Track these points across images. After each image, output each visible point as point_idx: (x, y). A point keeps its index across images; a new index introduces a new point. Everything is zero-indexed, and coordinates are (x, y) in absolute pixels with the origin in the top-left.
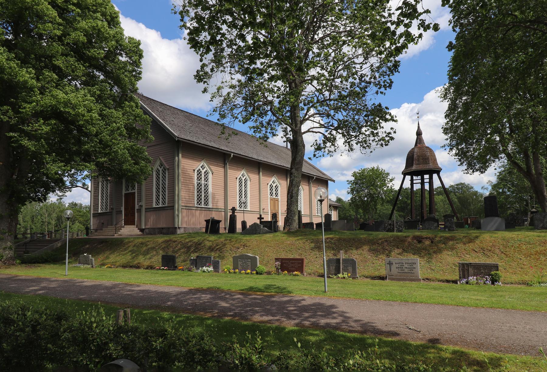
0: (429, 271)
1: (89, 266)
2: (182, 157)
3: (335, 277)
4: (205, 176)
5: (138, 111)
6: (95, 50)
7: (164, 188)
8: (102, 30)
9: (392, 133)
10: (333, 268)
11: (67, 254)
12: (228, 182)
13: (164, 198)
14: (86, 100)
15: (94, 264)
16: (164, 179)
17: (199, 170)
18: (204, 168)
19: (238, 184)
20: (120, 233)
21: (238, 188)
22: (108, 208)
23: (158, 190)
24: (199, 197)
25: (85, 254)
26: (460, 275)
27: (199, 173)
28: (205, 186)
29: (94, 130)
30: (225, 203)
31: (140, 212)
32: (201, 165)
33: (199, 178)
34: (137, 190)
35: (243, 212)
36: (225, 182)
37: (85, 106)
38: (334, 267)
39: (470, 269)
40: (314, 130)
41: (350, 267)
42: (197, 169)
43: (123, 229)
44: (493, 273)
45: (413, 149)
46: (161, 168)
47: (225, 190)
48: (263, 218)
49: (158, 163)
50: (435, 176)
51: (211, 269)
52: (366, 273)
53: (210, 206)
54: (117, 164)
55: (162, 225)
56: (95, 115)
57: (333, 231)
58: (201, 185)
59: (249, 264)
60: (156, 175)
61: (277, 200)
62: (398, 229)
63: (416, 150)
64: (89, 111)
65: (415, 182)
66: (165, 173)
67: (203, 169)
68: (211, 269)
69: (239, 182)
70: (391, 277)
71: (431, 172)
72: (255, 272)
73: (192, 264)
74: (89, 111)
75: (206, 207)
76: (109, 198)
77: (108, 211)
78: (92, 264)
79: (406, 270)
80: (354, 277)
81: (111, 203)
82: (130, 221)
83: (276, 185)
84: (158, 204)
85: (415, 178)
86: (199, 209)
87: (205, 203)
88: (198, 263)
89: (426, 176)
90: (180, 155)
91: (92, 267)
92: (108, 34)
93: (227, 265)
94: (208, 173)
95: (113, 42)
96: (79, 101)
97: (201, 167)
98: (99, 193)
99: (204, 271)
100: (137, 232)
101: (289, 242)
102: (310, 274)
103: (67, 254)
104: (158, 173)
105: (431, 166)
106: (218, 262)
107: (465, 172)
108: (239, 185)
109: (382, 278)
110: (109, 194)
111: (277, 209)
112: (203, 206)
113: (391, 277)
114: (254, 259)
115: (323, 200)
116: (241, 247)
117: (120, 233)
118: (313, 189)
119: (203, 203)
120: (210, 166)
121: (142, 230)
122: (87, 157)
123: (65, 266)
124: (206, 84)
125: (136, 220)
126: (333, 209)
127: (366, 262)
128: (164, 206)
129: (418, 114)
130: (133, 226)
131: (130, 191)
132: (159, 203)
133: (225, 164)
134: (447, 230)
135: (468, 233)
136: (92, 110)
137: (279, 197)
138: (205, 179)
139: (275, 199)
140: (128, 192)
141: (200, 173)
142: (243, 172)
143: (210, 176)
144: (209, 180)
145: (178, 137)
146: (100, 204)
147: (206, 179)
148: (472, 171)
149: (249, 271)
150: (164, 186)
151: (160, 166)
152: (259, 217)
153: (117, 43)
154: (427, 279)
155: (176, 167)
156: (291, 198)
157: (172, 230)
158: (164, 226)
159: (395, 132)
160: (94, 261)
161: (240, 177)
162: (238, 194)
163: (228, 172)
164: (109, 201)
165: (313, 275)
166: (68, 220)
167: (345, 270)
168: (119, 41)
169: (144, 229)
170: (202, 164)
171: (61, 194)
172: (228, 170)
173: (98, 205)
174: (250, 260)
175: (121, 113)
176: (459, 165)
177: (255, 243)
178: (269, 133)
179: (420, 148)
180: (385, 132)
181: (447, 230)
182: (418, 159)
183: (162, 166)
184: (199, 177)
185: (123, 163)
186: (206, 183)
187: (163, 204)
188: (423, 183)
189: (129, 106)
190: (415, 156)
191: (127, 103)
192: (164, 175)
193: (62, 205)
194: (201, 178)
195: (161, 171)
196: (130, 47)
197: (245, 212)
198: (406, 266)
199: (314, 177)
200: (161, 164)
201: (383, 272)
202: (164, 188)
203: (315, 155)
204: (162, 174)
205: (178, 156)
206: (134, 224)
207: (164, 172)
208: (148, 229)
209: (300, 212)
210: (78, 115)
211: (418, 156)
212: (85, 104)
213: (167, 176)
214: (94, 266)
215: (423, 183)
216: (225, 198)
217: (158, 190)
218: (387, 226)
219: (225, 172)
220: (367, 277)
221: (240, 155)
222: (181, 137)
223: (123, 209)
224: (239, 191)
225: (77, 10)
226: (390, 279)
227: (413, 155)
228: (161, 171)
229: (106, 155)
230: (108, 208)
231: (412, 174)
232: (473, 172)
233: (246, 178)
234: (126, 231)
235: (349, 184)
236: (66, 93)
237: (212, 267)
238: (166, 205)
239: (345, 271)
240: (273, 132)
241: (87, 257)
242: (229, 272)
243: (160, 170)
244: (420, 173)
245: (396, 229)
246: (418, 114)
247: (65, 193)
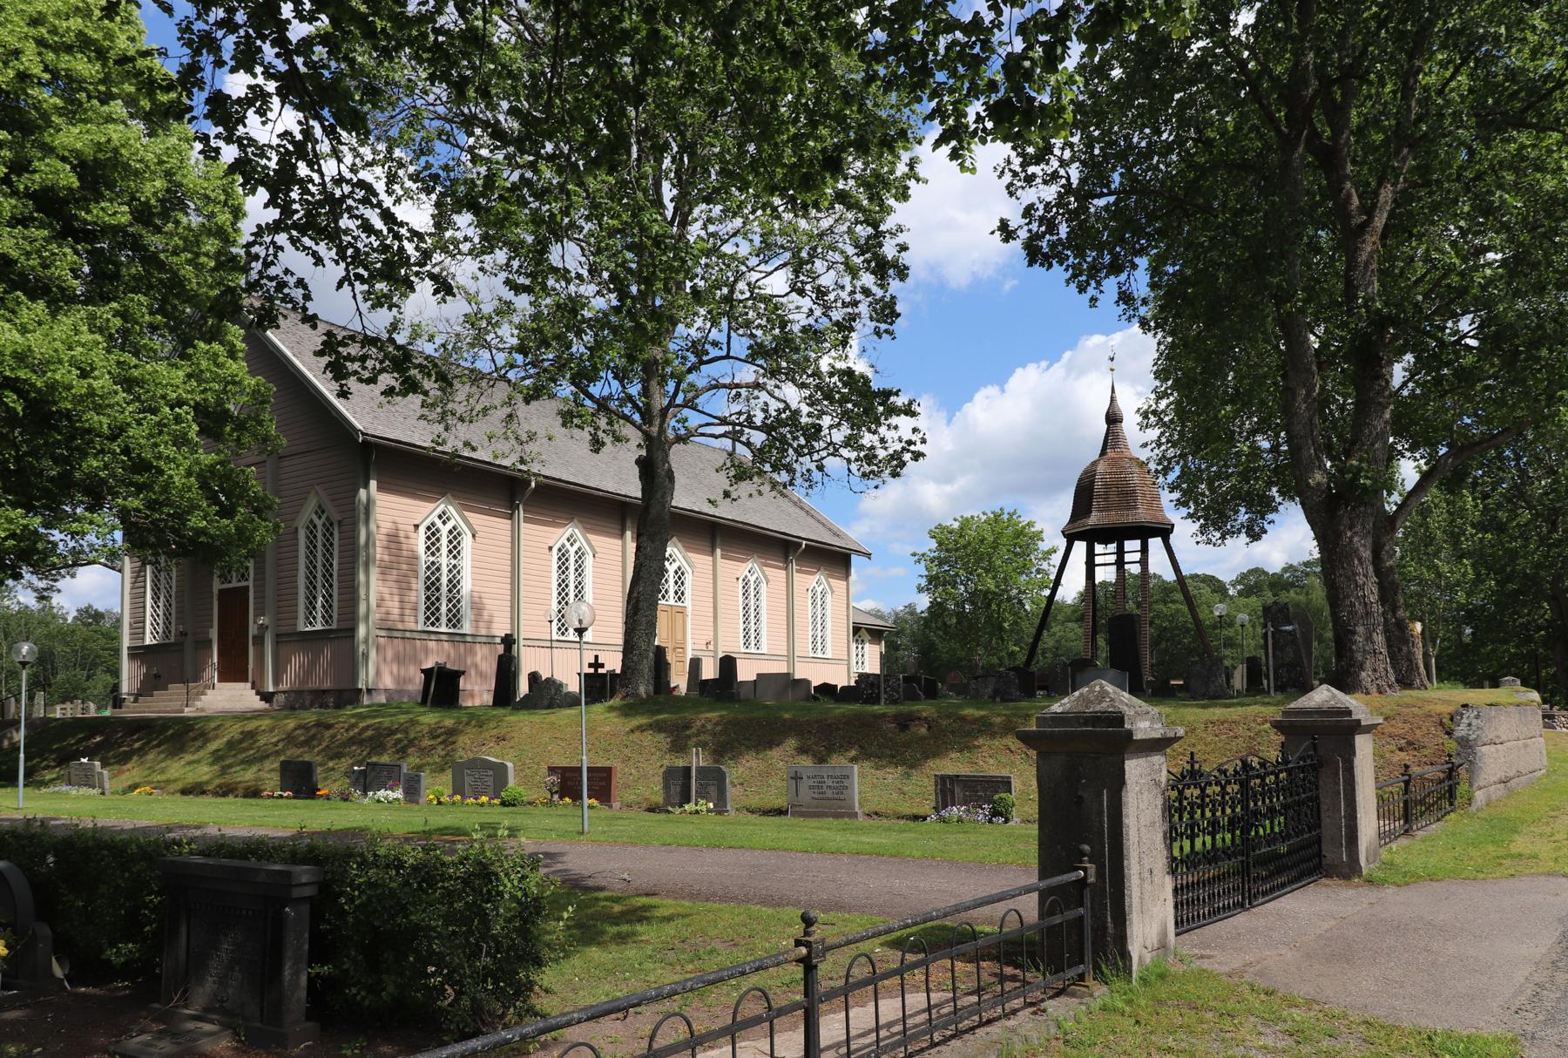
0: (895, 796)
1: (96, 791)
2: (380, 489)
4: (450, 542)
5: (234, 366)
6: (103, 204)
7: (328, 575)
8: (123, 151)
10: (676, 789)
11: (22, 755)
12: (522, 559)
13: (328, 607)
14: (79, 343)
15: (107, 786)
16: (328, 550)
17: (433, 524)
18: (448, 519)
20: (199, 704)
21: (555, 575)
22: (173, 632)
23: (311, 583)
24: (433, 604)
25: (85, 760)
27: (432, 533)
28: (450, 571)
29: (102, 422)
30: (512, 619)
31: (262, 644)
32: (439, 511)
34: (255, 580)
35: (578, 646)
36: (512, 560)
37: (73, 362)
38: (678, 789)
39: (957, 790)
41: (712, 788)
42: (427, 523)
45: (1094, 463)
46: (320, 518)
47: (512, 584)
48: (602, 666)
49: (312, 504)
50: (1155, 543)
51: (398, 794)
52: (755, 801)
53: (467, 628)
54: (169, 515)
58: (438, 569)
59: (490, 781)
60: (308, 537)
61: (682, 612)
62: (890, 696)
63: (1101, 468)
64: (84, 375)
65: (1098, 560)
66: (332, 534)
67: (444, 523)
68: (398, 794)
69: (560, 559)
72: (496, 801)
74: (84, 375)
75: (451, 631)
76: (173, 603)
77: (173, 640)
78: (101, 786)
79: (829, 793)
81: (180, 620)
82: (233, 670)
83: (679, 568)
84: (311, 623)
85: (1099, 548)
86: (433, 637)
88: (367, 780)
89: (1132, 545)
91: (103, 793)
92: (141, 161)
94: (459, 534)
95: (158, 184)
96: (56, 351)
98: (145, 587)
100: (256, 703)
101: (608, 729)
102: (629, 806)
103: (22, 755)
104: (311, 532)
105: (1142, 515)
106: (417, 780)
107: (1199, 539)
108: (560, 568)
109: (780, 812)
110: (174, 589)
111: (679, 636)
112: (443, 629)
114: (500, 770)
115: (586, 629)
117: (199, 704)
118: (799, 578)
119: (444, 620)
120: (466, 513)
121: (266, 697)
123: (15, 789)
125: (251, 666)
126: (867, 637)
128: (327, 627)
129: (1112, 359)
130: (242, 685)
131: (234, 584)
132: (314, 618)
134: (998, 699)
135: (1016, 708)
137: (688, 601)
138: (450, 552)
139: (675, 609)
140: (230, 586)
141: (433, 534)
142: (570, 530)
144: (463, 553)
145: (363, 434)
146: (148, 619)
147: (454, 551)
148: (1218, 535)
149: (484, 799)
151: (316, 513)
154: (876, 814)
156: (635, 614)
157: (348, 695)
158: (327, 685)
159: (924, 441)
160: (106, 779)
161: (563, 546)
162: (555, 593)
163: (522, 531)
164: (173, 612)
165: (636, 808)
166: (24, 668)
167: (702, 794)
168: (174, 174)
170: (442, 507)
171: (42, 584)
172: (523, 524)
173: (144, 622)
174: (491, 773)
176: (868, 555)
177: (526, 730)
179: (1114, 463)
180: (900, 440)
181: (998, 699)
182: (1106, 493)
183: (323, 512)
184: (433, 544)
187: (327, 622)
188: (1120, 563)
190: (1098, 484)
192: (328, 540)
193: (54, 617)
194: (438, 550)
195: (320, 528)
197: (549, 644)
199: (800, 544)
200: (320, 507)
201: (780, 802)
202: (328, 575)
203: (727, 494)
204: (324, 535)
205: (366, 486)
206: (246, 680)
207: (328, 530)
208: (284, 692)
209: (660, 651)
210: (52, 386)
211: (1106, 485)
212: (73, 356)
213: (336, 542)
216: (512, 607)
217: (311, 583)
219: (513, 531)
220: (752, 812)
221: (560, 480)
224: (560, 585)
225: (51, 101)
226: (793, 814)
227: (1093, 482)
228: (320, 528)
230: (173, 632)
231: (1094, 537)
232: (1223, 537)
233: (580, 549)
235: (919, 561)
236: (24, 330)
237: (401, 790)
238: (334, 626)
239: (703, 798)
240: (614, 432)
241: (88, 769)
242: (440, 803)
243: (319, 523)
244: (1115, 535)
245: (883, 696)
246: (1112, 359)
247: (56, 581)
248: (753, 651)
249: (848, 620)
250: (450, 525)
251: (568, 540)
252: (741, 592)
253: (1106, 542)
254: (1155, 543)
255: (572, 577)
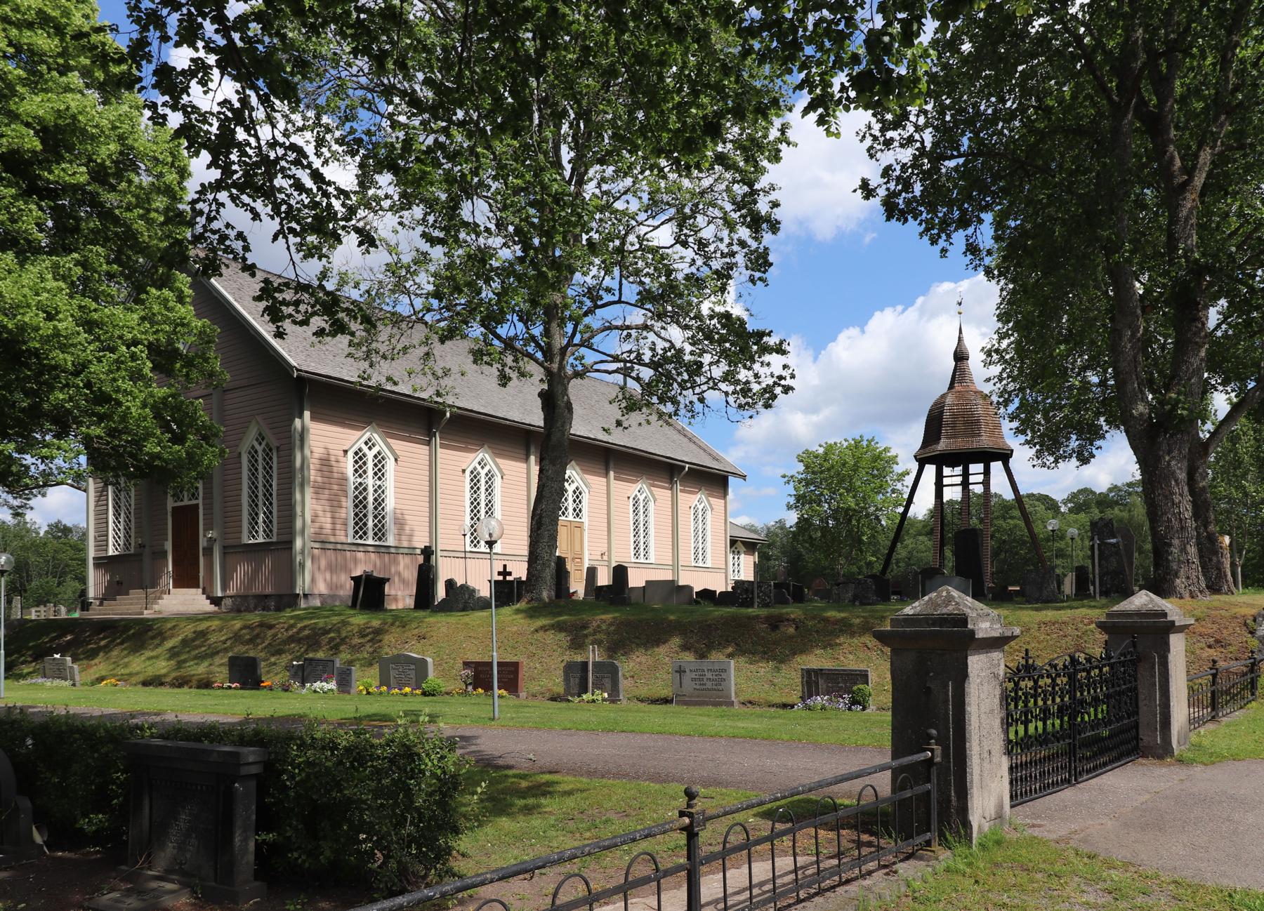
1: (68, 683)
3: (577, 699)
5: (183, 310)
6: (63, 166)
9: (788, 378)
10: (575, 681)
15: (77, 678)
17: (360, 450)
19: (468, 487)
24: (361, 519)
26: (803, 692)
27: (360, 458)
29: (67, 360)
31: (211, 555)
33: (360, 469)
35: (488, 556)
37: (40, 306)
38: (577, 680)
40: (596, 367)
41: (607, 680)
42: (355, 448)
43: (165, 596)
44: (855, 688)
45: (943, 396)
46: (260, 444)
48: (510, 574)
50: (997, 467)
51: (332, 685)
52: (644, 692)
53: (391, 541)
54: (127, 441)
55: (265, 586)
56: (66, 324)
57: (629, 604)
60: (250, 461)
61: (580, 526)
63: (949, 400)
64: (50, 317)
65: (946, 481)
66: (271, 459)
68: (332, 685)
70: (682, 698)
71: (986, 457)
72: (418, 692)
73: (294, 676)
74: (50, 317)
77: (132, 551)
78: (73, 679)
79: (709, 685)
80: (614, 699)
82: (186, 578)
83: (577, 488)
84: (253, 536)
85: (947, 471)
86: (361, 549)
87: (375, 534)
88: (305, 673)
89: (976, 468)
90: (307, 414)
91: (74, 685)
92: (96, 126)
93: (365, 678)
95: (112, 147)
97: (366, 443)
98: (107, 505)
99: (315, 691)
100: (206, 606)
101: (515, 629)
102: (534, 696)
105: (985, 441)
107: (1035, 463)
109: (666, 701)
110: (133, 507)
111: (577, 548)
112: (370, 542)
113: (682, 698)
114: (421, 666)
115: (496, 542)
116: (413, 640)
119: (370, 533)
121: (215, 601)
122: (63, 423)
124: (324, 260)
125: (201, 574)
127: (656, 668)
128: (268, 540)
131: (186, 502)
132: (257, 532)
133: (431, 435)
134: (857, 603)
136: (58, 313)
137: (585, 518)
141: (361, 458)
143: (390, 465)
144: (387, 475)
145: (298, 370)
147: (379, 473)
148: (1052, 459)
149: (407, 690)
150: (268, 490)
151: (257, 440)
152: (502, 570)
153: (123, 145)
154: (750, 702)
155: (298, 443)
156: (539, 529)
157: (288, 599)
158: (269, 590)
160: (76, 672)
162: (468, 510)
164: (133, 526)
167: (599, 685)
168: (126, 138)
169: (221, 598)
171: (16, 503)
172: (439, 450)
173: (107, 536)
174: (413, 667)
175: (135, 316)
176: (744, 477)
177: (444, 629)
178: (510, 368)
181: (857, 603)
182: (954, 423)
183: (263, 439)
185: (145, 440)
186: (378, 483)
187: (268, 536)
188: (965, 484)
189: (159, 297)
190: (947, 415)
191: (154, 291)
192: (268, 463)
193: (28, 531)
194: (365, 472)
195: (260, 452)
196: (154, 152)
198: (709, 675)
199: (684, 467)
200: (260, 434)
203: (619, 423)
204: (264, 459)
206: (197, 586)
207: (267, 455)
208: (231, 597)
210: (22, 328)
211: (954, 416)
212: (39, 301)
213: (275, 466)
214: (77, 684)
215: (965, 484)
217: (253, 501)
218: (741, 594)
219: (430, 455)
220: (642, 701)
222: (578, 433)
223: (169, 546)
224: (472, 503)
226: (678, 703)
227: (942, 412)
228: (260, 452)
229: (101, 418)
231: (942, 461)
234: (174, 602)
235: (788, 482)
237: (334, 682)
238: (274, 539)
240: (519, 368)
241: (61, 663)
242: (368, 693)
243: (259, 449)
244: (961, 459)
247: (29, 499)
248: (642, 560)
249: (726, 534)
250: (375, 450)
251: (480, 463)
252: (692, 517)
253: (953, 466)
254: (997, 467)
255: (483, 497)
